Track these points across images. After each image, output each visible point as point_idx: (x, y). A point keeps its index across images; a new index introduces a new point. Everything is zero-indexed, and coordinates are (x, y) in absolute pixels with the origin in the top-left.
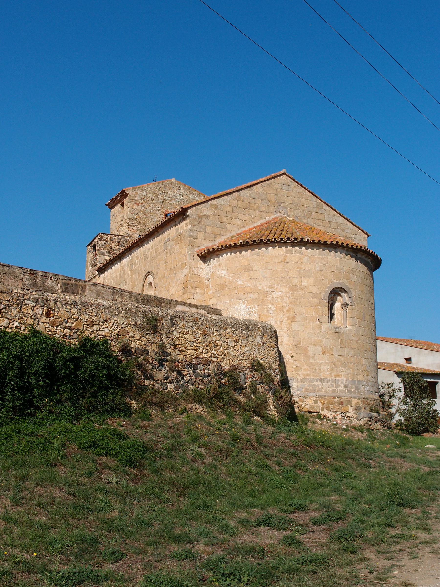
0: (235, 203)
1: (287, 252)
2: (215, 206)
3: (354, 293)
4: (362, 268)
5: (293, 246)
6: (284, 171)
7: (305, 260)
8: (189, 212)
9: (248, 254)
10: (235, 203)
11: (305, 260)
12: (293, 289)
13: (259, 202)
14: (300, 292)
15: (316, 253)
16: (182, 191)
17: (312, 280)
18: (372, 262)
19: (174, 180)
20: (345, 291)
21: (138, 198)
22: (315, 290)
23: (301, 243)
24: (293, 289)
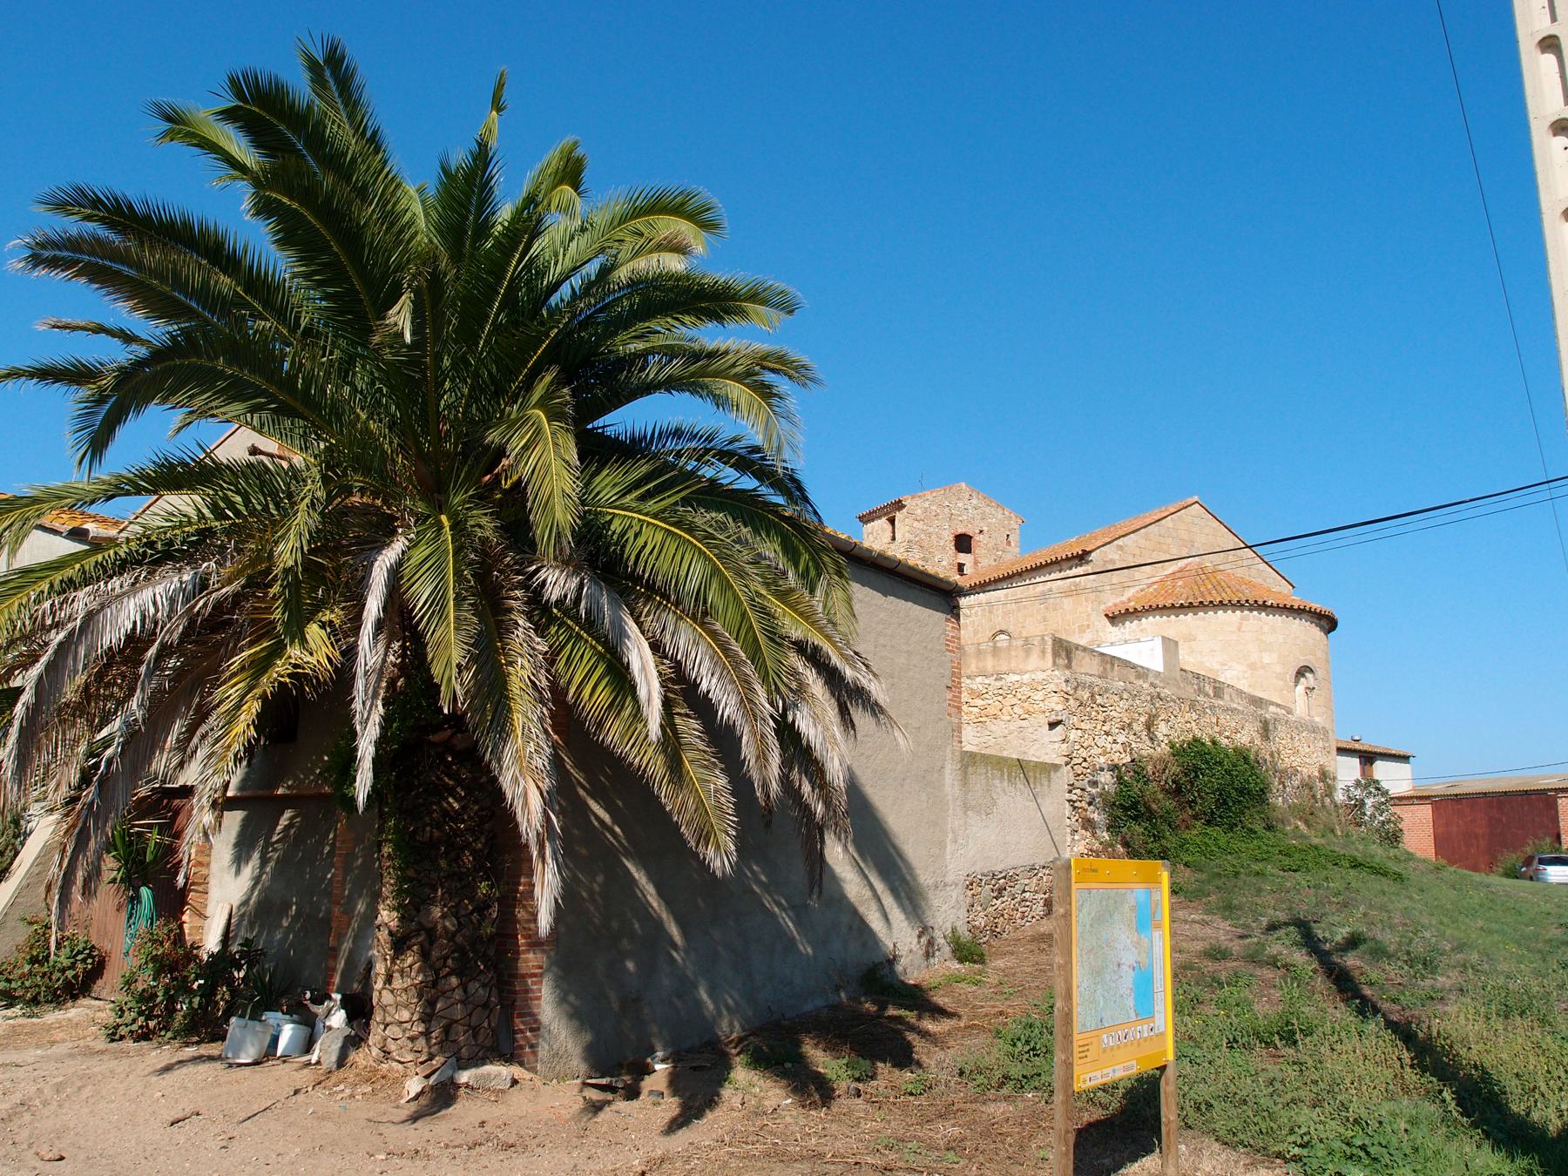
0: (1142, 542)
1: (1242, 618)
2: (1120, 548)
3: (1320, 673)
4: (1314, 632)
5: (1251, 610)
6: (1196, 498)
7: (1266, 628)
8: (1093, 556)
9: (1188, 618)
10: (1142, 542)
11: (1266, 628)
12: (1252, 667)
13: (1169, 541)
14: (1261, 672)
15: (1278, 620)
16: (974, 501)
17: (1275, 655)
18: (1328, 623)
19: (963, 485)
20: (1311, 671)
21: (919, 511)
22: (1278, 669)
23: (1263, 607)
24: (1252, 667)
